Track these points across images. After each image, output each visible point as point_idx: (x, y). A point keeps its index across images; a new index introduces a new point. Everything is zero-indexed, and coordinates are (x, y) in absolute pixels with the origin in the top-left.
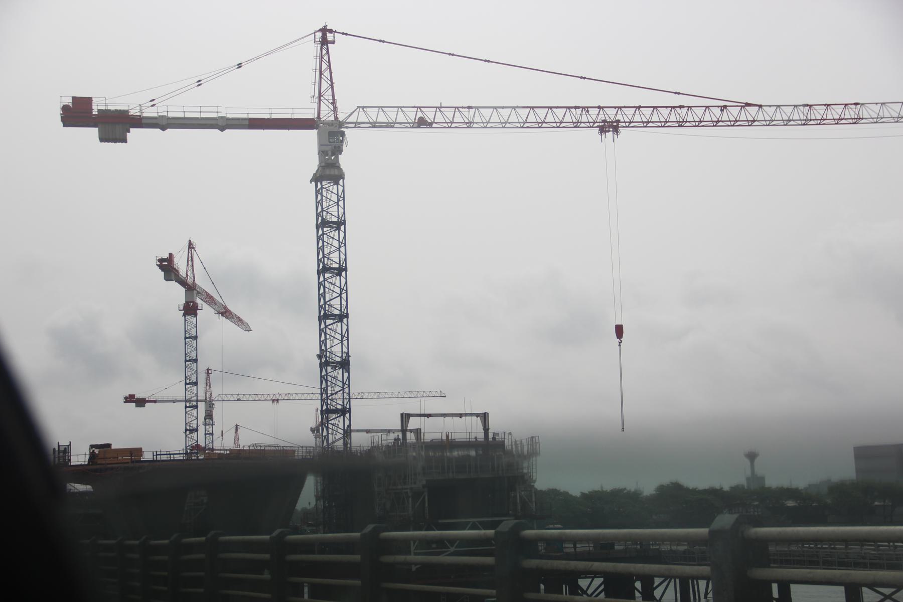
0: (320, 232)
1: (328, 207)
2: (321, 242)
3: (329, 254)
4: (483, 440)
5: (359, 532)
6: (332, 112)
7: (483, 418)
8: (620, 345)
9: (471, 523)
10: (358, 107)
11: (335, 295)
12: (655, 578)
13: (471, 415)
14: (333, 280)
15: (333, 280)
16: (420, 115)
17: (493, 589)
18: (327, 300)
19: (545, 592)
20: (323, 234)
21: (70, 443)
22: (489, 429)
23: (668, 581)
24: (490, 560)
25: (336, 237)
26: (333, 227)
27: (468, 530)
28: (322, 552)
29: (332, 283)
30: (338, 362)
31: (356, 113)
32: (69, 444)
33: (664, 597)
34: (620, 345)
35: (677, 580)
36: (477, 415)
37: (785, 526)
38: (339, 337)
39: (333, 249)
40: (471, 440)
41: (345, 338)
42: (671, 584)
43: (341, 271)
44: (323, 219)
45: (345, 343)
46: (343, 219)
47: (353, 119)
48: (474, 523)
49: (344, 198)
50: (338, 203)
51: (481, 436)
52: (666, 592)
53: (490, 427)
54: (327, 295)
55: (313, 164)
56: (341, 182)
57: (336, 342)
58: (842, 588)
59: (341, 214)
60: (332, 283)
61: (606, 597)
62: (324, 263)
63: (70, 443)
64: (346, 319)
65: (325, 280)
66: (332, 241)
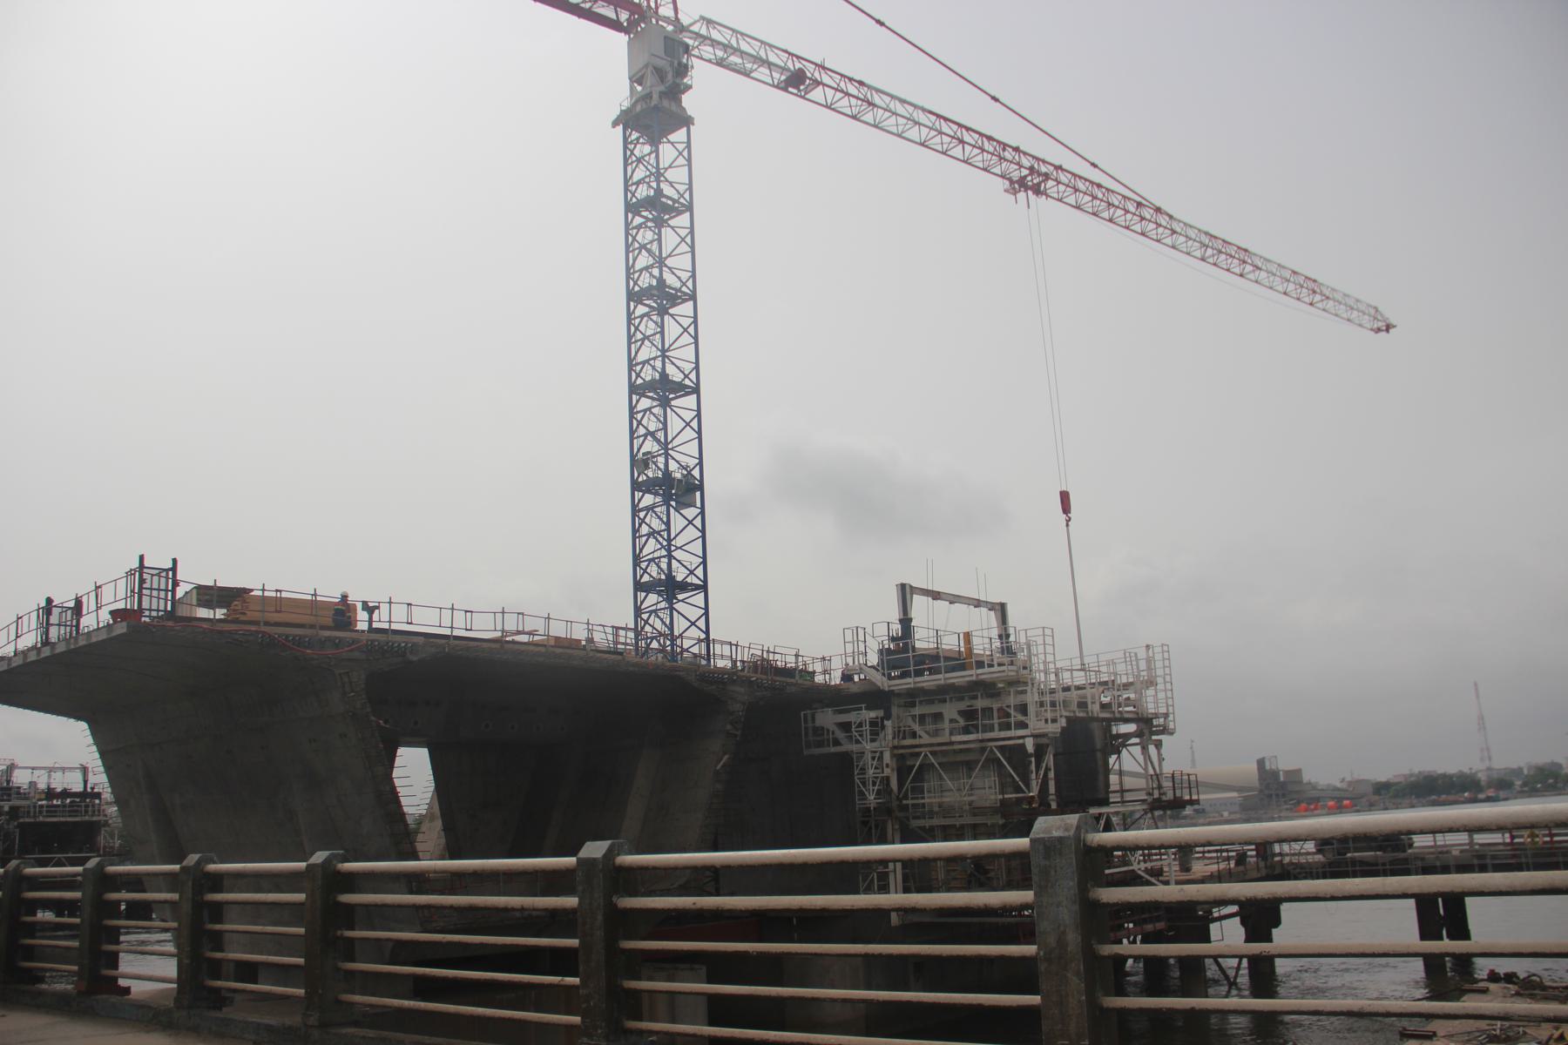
5: (81, 866)
7: (999, 613)
8: (1067, 525)
10: (703, 18)
12: (1466, 898)
13: (978, 603)
16: (798, 66)
19: (1141, 943)
21: (175, 561)
24: (571, 901)
27: (52, 867)
31: (699, 24)
32: (169, 565)
34: (1067, 525)
36: (992, 607)
47: (695, 28)
48: (59, 858)
55: (618, 93)
58: (1411, 902)
61: (1248, 940)
63: (175, 561)
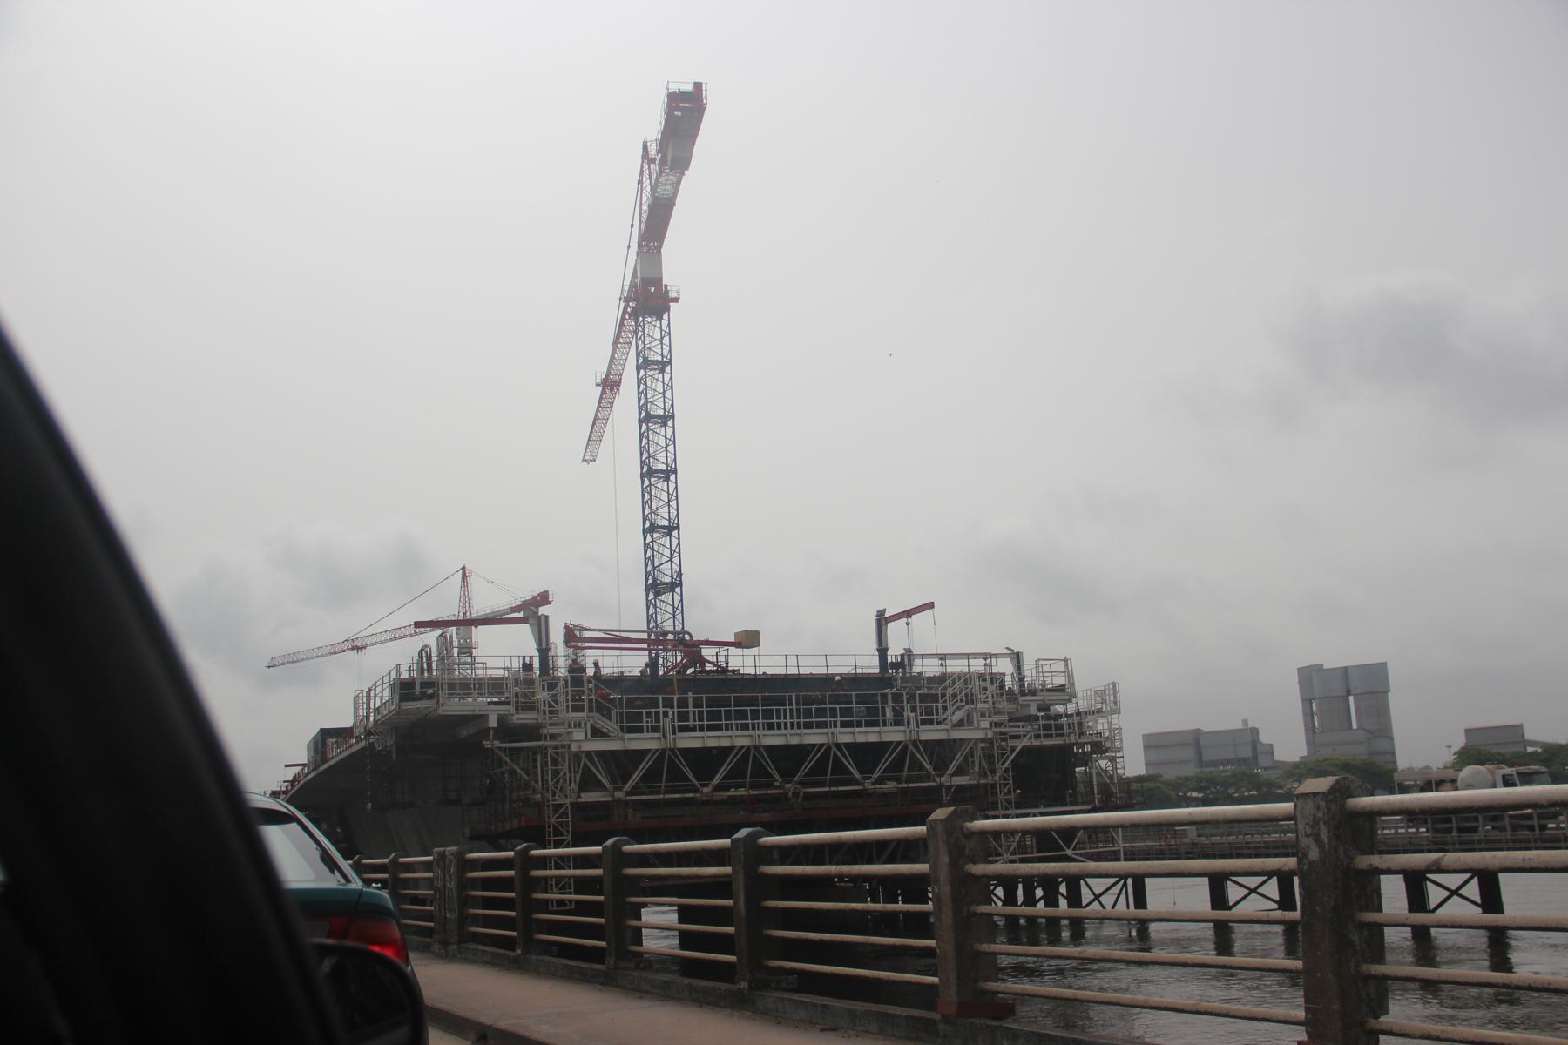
0: (646, 483)
1: (657, 509)
2: (649, 551)
3: (657, 509)
4: (877, 671)
6: (661, 395)
9: (951, 769)
11: (666, 559)
14: (662, 541)
15: (662, 541)
17: (602, 918)
18: (656, 564)
20: (650, 485)
22: (887, 649)
23: (994, 898)
25: (665, 489)
26: (661, 478)
28: (558, 867)
29: (664, 602)
30: (667, 584)
33: (1439, 910)
35: (1130, 881)
37: (1107, 812)
38: (670, 609)
39: (662, 503)
40: (859, 671)
41: (678, 612)
42: (1238, 881)
43: (672, 529)
44: (652, 524)
45: (679, 617)
46: (673, 466)
49: (677, 497)
50: (666, 448)
51: (871, 665)
52: (1466, 895)
53: (889, 646)
54: (656, 560)
56: (665, 316)
57: (662, 503)
59: (668, 406)
60: (664, 602)
62: (649, 465)
64: (676, 531)
65: (653, 541)
66: (661, 494)
